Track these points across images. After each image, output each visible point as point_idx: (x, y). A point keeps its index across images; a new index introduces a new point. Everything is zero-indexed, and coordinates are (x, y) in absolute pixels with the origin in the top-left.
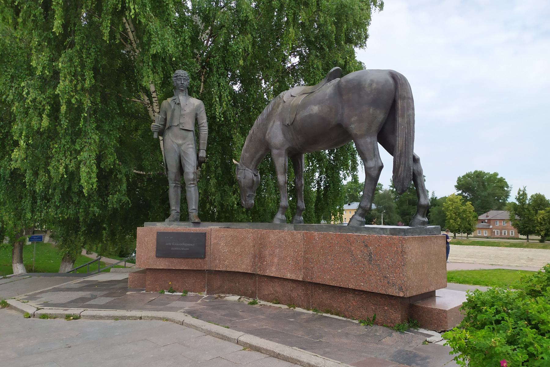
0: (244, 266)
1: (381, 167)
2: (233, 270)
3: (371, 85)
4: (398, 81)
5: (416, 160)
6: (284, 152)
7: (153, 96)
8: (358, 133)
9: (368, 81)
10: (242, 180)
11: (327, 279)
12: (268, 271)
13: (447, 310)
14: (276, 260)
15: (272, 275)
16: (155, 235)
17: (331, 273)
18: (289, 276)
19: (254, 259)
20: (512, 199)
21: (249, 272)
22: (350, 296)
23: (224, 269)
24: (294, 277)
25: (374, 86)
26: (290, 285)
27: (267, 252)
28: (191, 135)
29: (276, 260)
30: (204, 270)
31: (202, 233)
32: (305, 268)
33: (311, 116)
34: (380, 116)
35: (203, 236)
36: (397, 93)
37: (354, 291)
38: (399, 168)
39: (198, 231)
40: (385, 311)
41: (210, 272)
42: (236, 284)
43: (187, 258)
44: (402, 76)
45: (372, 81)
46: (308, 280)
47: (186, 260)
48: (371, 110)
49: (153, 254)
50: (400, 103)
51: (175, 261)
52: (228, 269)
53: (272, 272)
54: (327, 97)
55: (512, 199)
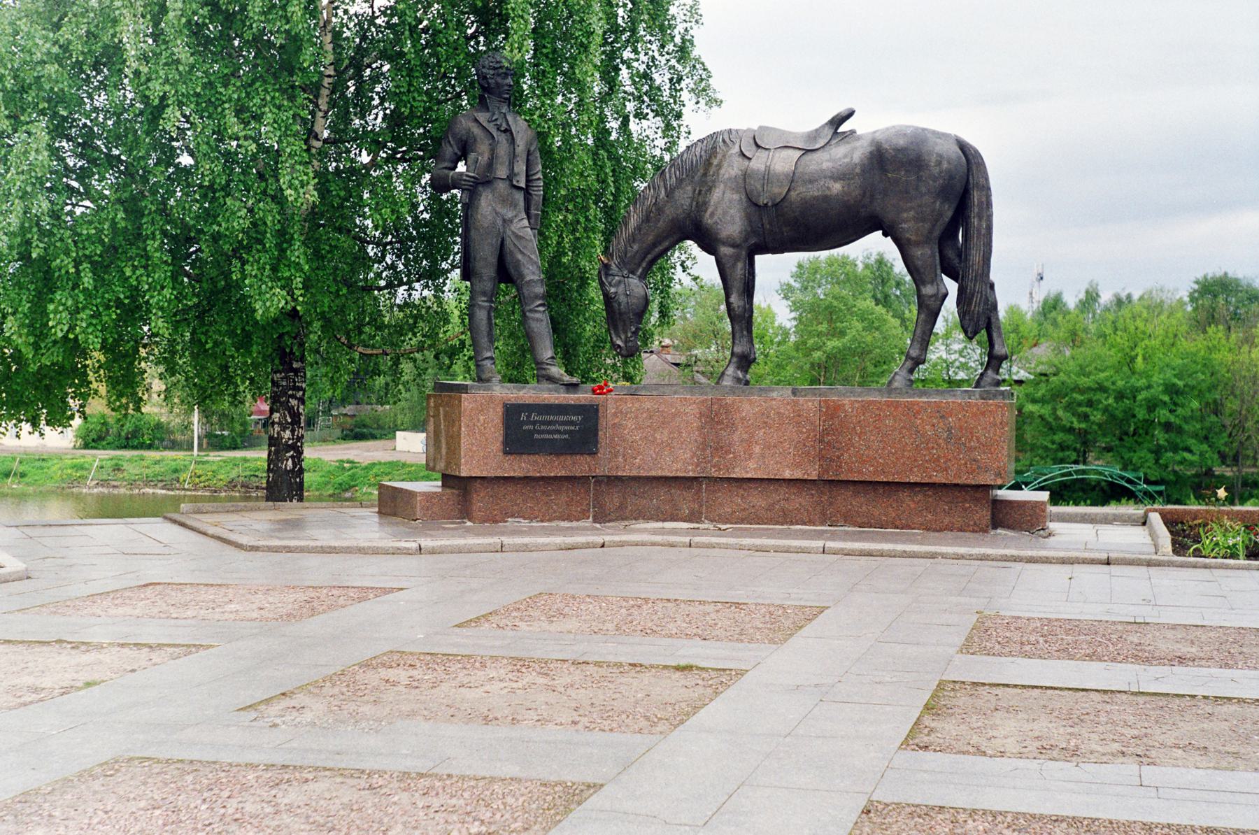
1: (946, 295)
3: (939, 163)
5: (992, 286)
8: (913, 238)
9: (934, 158)
10: (622, 299)
12: (737, 470)
14: (757, 449)
15: (749, 476)
16: (500, 410)
18: (787, 474)
19: (704, 450)
20: (776, 324)
21: (691, 474)
22: (905, 495)
23: (634, 473)
24: (798, 474)
25: (945, 165)
26: (783, 490)
27: (736, 437)
28: (520, 197)
29: (757, 449)
31: (592, 406)
32: (822, 458)
33: (826, 198)
40: (965, 510)
41: (599, 480)
42: (651, 500)
44: (976, 151)
46: (831, 476)
47: (562, 458)
49: (496, 445)
50: (976, 196)
51: (541, 459)
53: (751, 469)
54: (858, 170)
55: (776, 324)
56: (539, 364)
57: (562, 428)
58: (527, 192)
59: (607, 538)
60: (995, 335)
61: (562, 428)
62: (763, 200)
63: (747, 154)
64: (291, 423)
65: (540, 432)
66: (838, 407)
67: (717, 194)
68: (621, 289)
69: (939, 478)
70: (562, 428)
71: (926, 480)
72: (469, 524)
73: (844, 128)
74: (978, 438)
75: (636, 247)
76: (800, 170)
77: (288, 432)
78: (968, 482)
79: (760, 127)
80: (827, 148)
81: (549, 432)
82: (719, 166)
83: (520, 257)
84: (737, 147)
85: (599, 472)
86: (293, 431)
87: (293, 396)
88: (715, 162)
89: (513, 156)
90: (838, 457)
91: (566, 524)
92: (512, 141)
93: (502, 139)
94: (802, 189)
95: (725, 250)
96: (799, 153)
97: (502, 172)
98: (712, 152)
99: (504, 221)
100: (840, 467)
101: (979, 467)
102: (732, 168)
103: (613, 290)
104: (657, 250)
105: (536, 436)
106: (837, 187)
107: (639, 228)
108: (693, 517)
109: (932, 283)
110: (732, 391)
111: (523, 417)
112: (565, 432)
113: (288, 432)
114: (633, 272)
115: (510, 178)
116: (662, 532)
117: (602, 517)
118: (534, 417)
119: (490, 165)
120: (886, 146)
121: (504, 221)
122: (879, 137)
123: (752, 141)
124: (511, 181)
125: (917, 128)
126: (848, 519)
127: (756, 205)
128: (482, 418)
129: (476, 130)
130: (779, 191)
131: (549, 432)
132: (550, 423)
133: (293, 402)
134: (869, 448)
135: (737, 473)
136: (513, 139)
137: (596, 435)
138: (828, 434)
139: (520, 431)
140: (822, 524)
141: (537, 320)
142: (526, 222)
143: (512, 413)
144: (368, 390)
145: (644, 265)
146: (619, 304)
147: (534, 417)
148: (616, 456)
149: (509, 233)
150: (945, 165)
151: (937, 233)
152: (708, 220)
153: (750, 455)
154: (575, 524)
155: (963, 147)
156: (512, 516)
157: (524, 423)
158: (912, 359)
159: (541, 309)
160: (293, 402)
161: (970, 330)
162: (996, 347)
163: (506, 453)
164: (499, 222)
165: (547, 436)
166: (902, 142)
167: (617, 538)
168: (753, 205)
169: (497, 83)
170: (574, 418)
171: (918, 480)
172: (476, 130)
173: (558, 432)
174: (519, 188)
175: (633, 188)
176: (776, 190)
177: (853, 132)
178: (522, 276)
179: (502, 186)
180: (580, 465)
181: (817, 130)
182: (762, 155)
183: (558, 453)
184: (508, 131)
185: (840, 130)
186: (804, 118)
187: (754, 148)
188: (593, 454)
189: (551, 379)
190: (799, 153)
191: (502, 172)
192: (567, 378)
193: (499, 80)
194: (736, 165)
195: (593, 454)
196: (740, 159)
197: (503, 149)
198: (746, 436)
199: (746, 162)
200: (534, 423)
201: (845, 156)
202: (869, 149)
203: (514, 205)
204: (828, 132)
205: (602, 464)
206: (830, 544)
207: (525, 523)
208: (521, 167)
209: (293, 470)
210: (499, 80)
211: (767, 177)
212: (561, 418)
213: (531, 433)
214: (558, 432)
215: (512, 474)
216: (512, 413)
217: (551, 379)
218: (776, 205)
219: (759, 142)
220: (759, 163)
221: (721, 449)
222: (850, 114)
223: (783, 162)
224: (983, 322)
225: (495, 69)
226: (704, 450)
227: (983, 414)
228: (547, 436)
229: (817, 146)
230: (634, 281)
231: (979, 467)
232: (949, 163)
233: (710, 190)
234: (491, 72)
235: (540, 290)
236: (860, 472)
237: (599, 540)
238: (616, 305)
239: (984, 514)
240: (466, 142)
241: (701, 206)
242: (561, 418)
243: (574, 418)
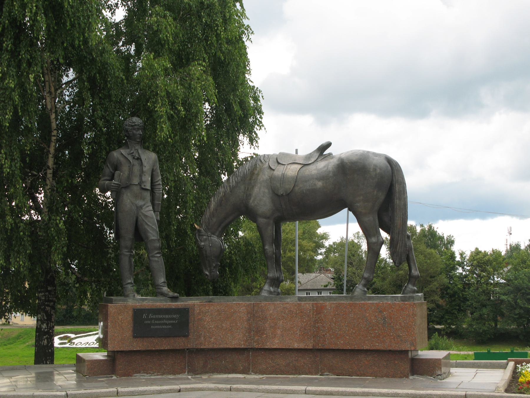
0: (236, 340)
2: (222, 346)
3: (375, 170)
4: (394, 166)
6: (272, 222)
7: (53, 134)
11: (340, 344)
12: (268, 344)
13: (441, 358)
15: (275, 347)
16: (131, 313)
17: (345, 338)
18: (296, 346)
19: (250, 333)
21: (243, 346)
23: (211, 346)
24: (302, 346)
25: (378, 171)
27: (267, 325)
28: (148, 195)
29: (279, 332)
30: (184, 349)
31: (185, 309)
34: (382, 196)
35: (185, 313)
36: (394, 178)
37: (367, 351)
38: (398, 243)
39: (180, 307)
43: (168, 337)
45: (376, 166)
46: (320, 346)
48: (375, 193)
49: (128, 333)
50: (397, 188)
51: (155, 340)
52: (216, 346)
53: (276, 344)
54: (331, 175)
56: (154, 285)
57: (168, 322)
58: (152, 191)
59: (182, 386)
60: (412, 264)
62: (281, 192)
63: (273, 167)
64: (47, 320)
67: (256, 190)
68: (207, 243)
69: (379, 346)
70: (168, 322)
72: (114, 377)
73: (326, 152)
74: (400, 324)
75: (214, 220)
76: (300, 174)
77: (45, 325)
78: (396, 348)
79: (280, 153)
80: (315, 163)
81: (159, 324)
82: (258, 174)
83: (146, 227)
84: (267, 163)
85: (189, 346)
86: (47, 324)
87: (48, 305)
88: (256, 172)
89: (142, 172)
90: (324, 335)
92: (141, 164)
93: (136, 163)
94: (301, 186)
95: (261, 220)
96: (300, 166)
97: (136, 181)
98: (255, 167)
99: (137, 207)
100: (325, 341)
101: (401, 340)
102: (265, 176)
103: (203, 244)
104: (227, 221)
106: (319, 184)
107: (216, 210)
108: (245, 371)
109: (374, 236)
110: (266, 299)
111: (144, 316)
112: (169, 324)
113: (45, 325)
114: (214, 234)
115: (140, 184)
116: (227, 381)
117: (194, 371)
118: (151, 316)
119: (129, 178)
120: (346, 161)
121: (137, 207)
122: (343, 156)
123: (275, 160)
124: (141, 185)
125: (364, 151)
126: (333, 370)
127: (277, 195)
129: (122, 159)
130: (289, 187)
131: (159, 324)
132: (160, 319)
133: (48, 308)
135: (268, 346)
136: (142, 163)
138: (318, 323)
139: (142, 323)
140: (316, 374)
141: (156, 261)
142: (151, 208)
143: (138, 314)
145: (220, 229)
146: (206, 251)
147: (151, 316)
149: (140, 214)
150: (378, 171)
151: (376, 208)
152: (252, 203)
153: (275, 335)
155: (390, 161)
158: (365, 279)
159: (158, 255)
160: (48, 308)
161: (397, 262)
162: (413, 271)
163: (134, 337)
164: (134, 208)
165: (158, 327)
166: (354, 159)
167: (188, 386)
168: (276, 195)
169: (133, 133)
170: (175, 316)
172: (122, 159)
173: (166, 324)
174: (147, 190)
176: (287, 187)
177: (330, 154)
178: (147, 238)
179: (136, 189)
180: (179, 343)
181: (310, 154)
182: (281, 168)
183: (166, 336)
184: (139, 159)
185: (325, 153)
186: (306, 147)
187: (277, 164)
188: (187, 336)
189: (163, 294)
190: (300, 166)
191: (136, 181)
192: (171, 294)
193: (134, 132)
194: (266, 173)
195: (187, 336)
196: (269, 170)
197: (136, 169)
198: (272, 325)
199: (272, 172)
200: (152, 319)
201: (325, 167)
202: (337, 163)
203: (143, 199)
204: (317, 155)
205: (191, 343)
206: (310, 388)
208: (147, 179)
209: (47, 345)
210: (134, 132)
211: (283, 178)
212: (167, 316)
214: (166, 324)
215: (138, 349)
216: (138, 314)
217: (163, 294)
218: (288, 195)
219: (279, 161)
220: (279, 171)
222: (329, 145)
223: (292, 170)
224: (404, 257)
225: (132, 126)
226: (250, 333)
228: (158, 327)
229: (310, 162)
230: (215, 238)
231: (401, 340)
232: (380, 169)
233: (253, 187)
234: (130, 128)
235: (158, 244)
237: (177, 387)
238: (204, 253)
239: (406, 366)
240: (117, 166)
241: (249, 196)
242: (167, 316)
243: (175, 316)
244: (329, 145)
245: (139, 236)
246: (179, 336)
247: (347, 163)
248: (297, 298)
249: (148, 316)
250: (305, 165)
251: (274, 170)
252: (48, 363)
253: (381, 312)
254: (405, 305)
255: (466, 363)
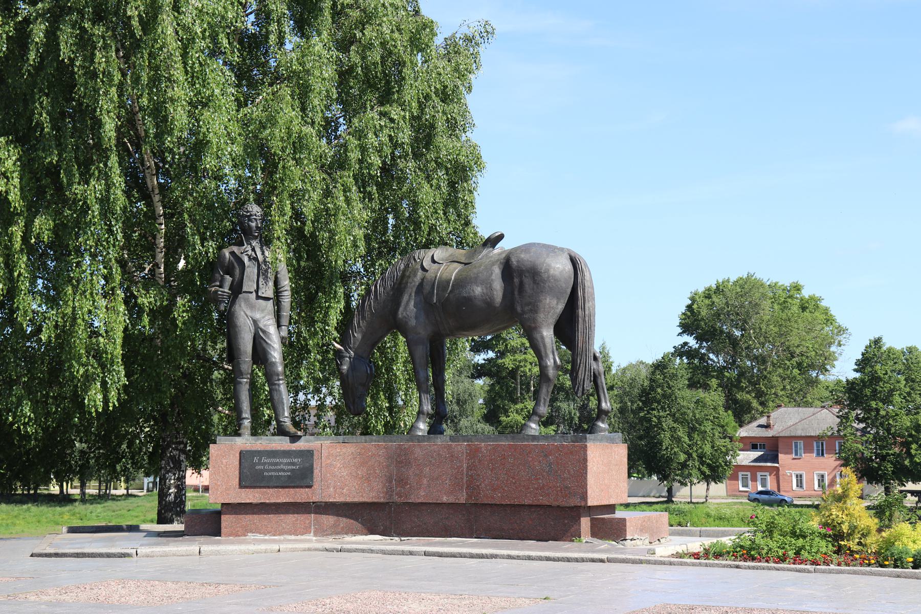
14: (425, 481)
15: (420, 501)
24: (451, 500)
29: (425, 481)
35: (308, 455)
37: (530, 506)
61: (285, 466)
65: (268, 471)
66: (478, 450)
69: (544, 501)
70: (286, 468)
71: (536, 503)
74: (569, 472)
81: (274, 470)
82: (409, 277)
91: (293, 537)
105: (266, 474)
111: (256, 460)
112: (288, 471)
118: (264, 460)
128: (224, 461)
131: (274, 470)
132: (276, 464)
134: (498, 479)
137: (312, 472)
143: (244, 456)
144: (400, 408)
147: (264, 460)
148: (328, 487)
154: (299, 537)
156: (251, 532)
157: (255, 464)
165: (273, 473)
170: (296, 460)
171: (530, 502)
173: (284, 471)
175: (19, 403)
198: (418, 472)
200: (265, 464)
207: (260, 537)
213: (262, 471)
214: (284, 471)
215: (248, 501)
216: (244, 456)
221: (402, 481)
222: (501, 237)
227: (571, 453)
228: (273, 473)
236: (493, 498)
242: (285, 461)
243: (296, 460)
244: (501, 237)
245: (260, 354)
246: (302, 487)
247: (556, 280)
248: (448, 438)
249: (260, 460)
250: (466, 264)
251: (427, 271)
252: (695, 481)
253: (546, 456)
254: (575, 447)
255: (518, 550)
